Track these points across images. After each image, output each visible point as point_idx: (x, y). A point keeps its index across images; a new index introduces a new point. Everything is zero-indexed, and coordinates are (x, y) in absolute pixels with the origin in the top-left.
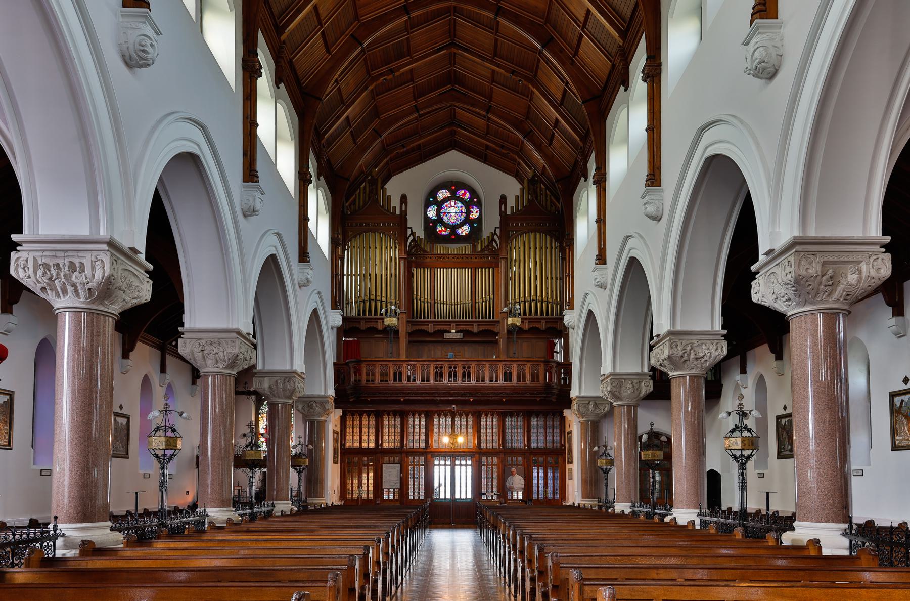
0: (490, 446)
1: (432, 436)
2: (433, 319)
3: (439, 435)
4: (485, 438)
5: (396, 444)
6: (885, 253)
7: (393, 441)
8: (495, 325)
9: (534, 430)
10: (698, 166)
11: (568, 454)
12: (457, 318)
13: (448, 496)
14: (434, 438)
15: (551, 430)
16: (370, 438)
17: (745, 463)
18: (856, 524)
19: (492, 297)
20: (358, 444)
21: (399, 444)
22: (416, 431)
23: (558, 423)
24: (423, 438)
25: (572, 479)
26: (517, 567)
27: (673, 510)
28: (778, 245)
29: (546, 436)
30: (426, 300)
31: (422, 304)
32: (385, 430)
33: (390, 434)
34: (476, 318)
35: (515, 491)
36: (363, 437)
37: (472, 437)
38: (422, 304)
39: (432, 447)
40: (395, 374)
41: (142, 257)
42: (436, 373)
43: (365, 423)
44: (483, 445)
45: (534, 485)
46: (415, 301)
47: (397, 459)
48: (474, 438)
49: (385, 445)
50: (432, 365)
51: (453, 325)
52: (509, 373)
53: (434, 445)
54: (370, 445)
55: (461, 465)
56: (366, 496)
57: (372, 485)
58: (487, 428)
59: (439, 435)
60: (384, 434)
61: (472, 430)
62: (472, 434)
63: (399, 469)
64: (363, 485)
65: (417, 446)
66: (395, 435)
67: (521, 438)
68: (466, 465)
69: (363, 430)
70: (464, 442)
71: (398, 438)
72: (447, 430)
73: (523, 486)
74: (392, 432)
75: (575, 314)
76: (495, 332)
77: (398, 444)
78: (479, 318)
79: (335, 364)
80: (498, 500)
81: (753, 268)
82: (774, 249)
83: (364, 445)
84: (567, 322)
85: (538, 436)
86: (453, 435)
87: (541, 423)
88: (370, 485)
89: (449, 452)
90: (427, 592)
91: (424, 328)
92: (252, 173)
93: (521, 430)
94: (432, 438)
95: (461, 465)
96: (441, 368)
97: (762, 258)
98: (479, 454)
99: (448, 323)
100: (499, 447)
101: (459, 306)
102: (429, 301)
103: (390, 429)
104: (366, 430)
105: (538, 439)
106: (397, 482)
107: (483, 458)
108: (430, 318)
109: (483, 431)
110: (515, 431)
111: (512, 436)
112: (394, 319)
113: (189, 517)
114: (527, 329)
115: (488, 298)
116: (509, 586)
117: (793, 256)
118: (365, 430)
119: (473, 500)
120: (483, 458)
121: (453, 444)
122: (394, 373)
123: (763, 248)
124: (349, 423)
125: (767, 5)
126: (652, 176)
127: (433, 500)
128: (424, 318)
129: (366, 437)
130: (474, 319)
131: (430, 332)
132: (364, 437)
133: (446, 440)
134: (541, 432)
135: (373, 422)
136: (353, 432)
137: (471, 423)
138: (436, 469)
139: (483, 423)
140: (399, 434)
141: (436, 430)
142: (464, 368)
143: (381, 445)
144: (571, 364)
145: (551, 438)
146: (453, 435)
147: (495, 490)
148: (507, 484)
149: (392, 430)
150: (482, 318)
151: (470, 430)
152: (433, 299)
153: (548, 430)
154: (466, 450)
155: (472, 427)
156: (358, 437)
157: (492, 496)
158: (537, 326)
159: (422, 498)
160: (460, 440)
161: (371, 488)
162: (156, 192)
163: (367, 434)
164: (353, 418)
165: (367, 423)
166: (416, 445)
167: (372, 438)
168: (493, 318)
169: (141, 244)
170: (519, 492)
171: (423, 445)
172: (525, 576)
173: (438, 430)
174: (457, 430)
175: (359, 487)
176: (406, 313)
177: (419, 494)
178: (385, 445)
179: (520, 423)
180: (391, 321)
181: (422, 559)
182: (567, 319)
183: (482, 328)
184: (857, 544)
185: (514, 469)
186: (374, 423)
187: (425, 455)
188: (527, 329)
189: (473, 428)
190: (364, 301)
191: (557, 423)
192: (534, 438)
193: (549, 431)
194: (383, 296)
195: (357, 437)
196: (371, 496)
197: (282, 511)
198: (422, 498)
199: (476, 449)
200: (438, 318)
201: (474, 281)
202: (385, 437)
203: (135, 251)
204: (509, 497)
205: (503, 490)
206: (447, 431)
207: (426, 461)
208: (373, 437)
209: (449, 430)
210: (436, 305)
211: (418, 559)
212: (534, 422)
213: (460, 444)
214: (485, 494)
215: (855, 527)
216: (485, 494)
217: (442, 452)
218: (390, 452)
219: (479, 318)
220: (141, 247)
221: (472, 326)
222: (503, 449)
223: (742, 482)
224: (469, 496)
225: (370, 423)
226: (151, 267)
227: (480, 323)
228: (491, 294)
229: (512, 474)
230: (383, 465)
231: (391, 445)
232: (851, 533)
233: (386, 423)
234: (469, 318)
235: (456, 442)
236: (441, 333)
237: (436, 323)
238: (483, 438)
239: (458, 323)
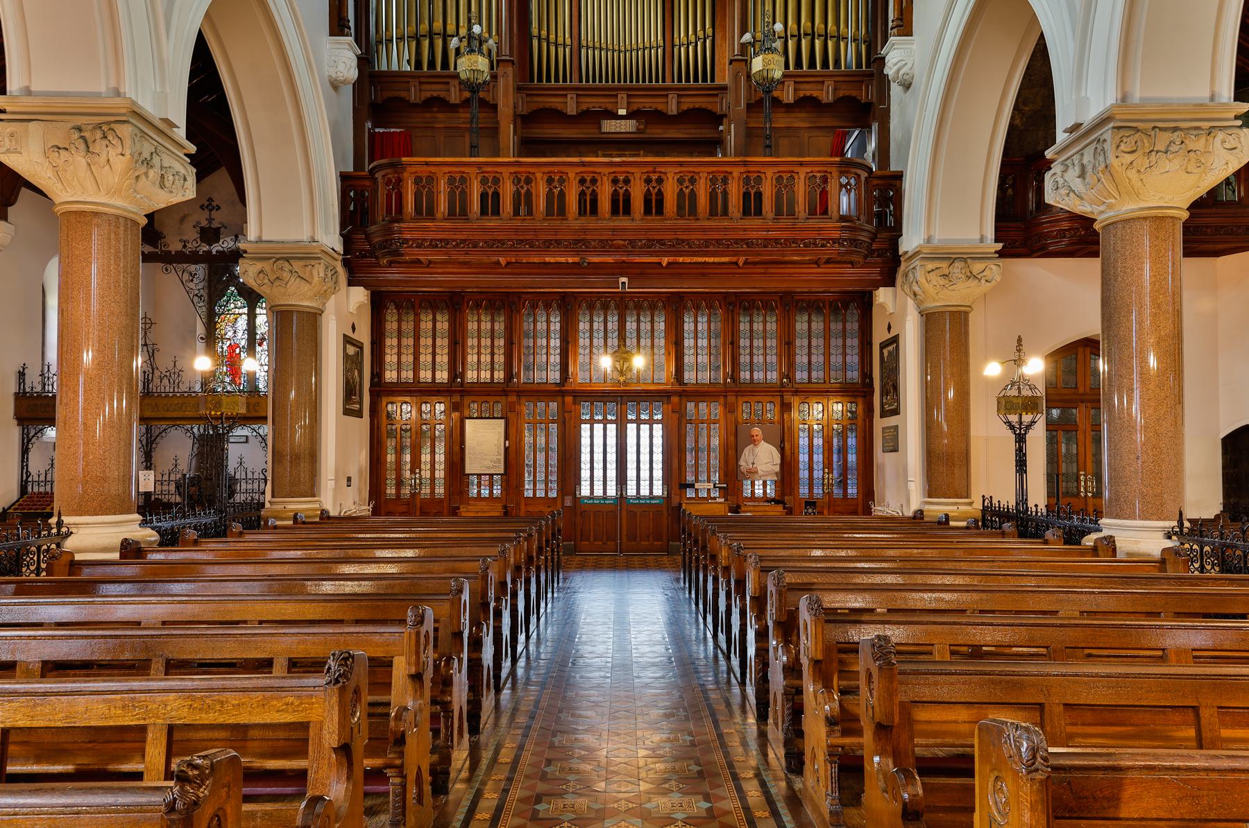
0: (705, 377)
1: (576, 354)
2: (576, 83)
3: (591, 352)
4: (692, 359)
5: (496, 374)
6: (1240, 127)
7: (489, 367)
8: (716, 95)
9: (801, 343)
10: (966, 8)
11: (884, 393)
12: (625, 81)
13: (612, 491)
14: (580, 359)
15: (840, 342)
16: (438, 358)
17: (1025, 434)
18: (1189, 520)
19: (709, 31)
20: (411, 374)
21: (502, 373)
22: (539, 344)
23: (856, 326)
24: (555, 359)
25: (895, 450)
26: (718, 589)
27: (1104, 521)
28: (1091, 114)
29: (827, 354)
30: (560, 40)
31: (553, 49)
32: (472, 342)
33: (483, 350)
34: (673, 82)
35: (747, 479)
36: (422, 358)
37: (663, 359)
38: (553, 49)
39: (575, 380)
40: (484, 196)
41: (181, 133)
42: (518, 193)
43: (426, 325)
44: (689, 376)
45: (801, 466)
46: (535, 42)
47: (498, 407)
48: (668, 360)
49: (471, 376)
50: (572, 175)
51: (622, 97)
52: (755, 193)
53: (580, 376)
54: (438, 375)
55: (639, 422)
56: (428, 491)
57: (442, 466)
58: (696, 338)
59: (591, 352)
60: (469, 350)
61: (663, 342)
62: (663, 351)
63: (502, 430)
64: (423, 466)
65: (541, 379)
66: (492, 354)
67: (772, 359)
68: (651, 422)
69: (422, 342)
70: (647, 368)
71: (500, 359)
72: (610, 341)
73: (777, 469)
74: (486, 346)
75: (914, 47)
76: (714, 114)
77: (499, 375)
78: (680, 80)
79: (344, 178)
80: (722, 500)
81: (1049, 154)
82: (907, 252)
83: (426, 375)
84: (895, 68)
85: (810, 354)
86: (622, 353)
87: (817, 325)
88: (437, 466)
89: (613, 392)
90: (561, 711)
91: (554, 102)
92: (341, 23)
93: (772, 343)
94: (575, 361)
95: (639, 422)
96: (594, 181)
97: (1061, 137)
98: (680, 396)
99: (612, 93)
100: (725, 380)
101: (634, 53)
102: (568, 41)
103: (483, 340)
104: (430, 341)
105: (810, 362)
106: (499, 460)
107: (688, 404)
108: (571, 81)
109: (688, 342)
110: (758, 343)
111: (751, 354)
112: (480, 59)
113: (184, 517)
114: (792, 102)
115: (700, 34)
116: (705, 619)
117: (1110, 131)
118: (426, 341)
119: (668, 498)
120: (688, 404)
121: (621, 373)
122: (482, 195)
123: (1063, 120)
124: (391, 325)
125: (904, 20)
126: (900, 23)
127: (577, 499)
128: (557, 80)
129: (429, 358)
130: (668, 83)
131: (569, 113)
132: (426, 358)
133: (606, 362)
134: (817, 346)
135: (443, 325)
136: (399, 346)
137: (661, 326)
138: (585, 428)
139: (688, 326)
140: (502, 351)
141: (583, 341)
142: (648, 181)
143: (463, 375)
144: (899, 176)
145: (840, 359)
146: (622, 353)
147: (716, 477)
148: (742, 462)
149: (486, 342)
150: (688, 80)
151: (661, 342)
152: (577, 39)
153: (833, 342)
154: (652, 388)
155: (663, 335)
156: (411, 359)
157: (709, 490)
158: (815, 94)
159: (553, 494)
160: (639, 362)
161: (440, 474)
162: (200, 37)
163: (430, 350)
164: (399, 315)
165: (430, 325)
166: (539, 376)
167: (443, 359)
168: (713, 80)
169: (178, 114)
170: (756, 483)
171: (555, 376)
172: (746, 625)
173: (587, 342)
174: (631, 342)
175: (412, 471)
176: (512, 62)
177: (546, 485)
178: (471, 376)
179: (772, 326)
180: (473, 65)
181: (550, 632)
182: (895, 61)
183: (688, 104)
184: (1191, 548)
185: (757, 431)
186: (446, 325)
187: (560, 398)
188: (792, 102)
189: (666, 338)
190: (417, 38)
191: (852, 326)
192: (801, 359)
193: (836, 342)
194: (461, 24)
195: (408, 359)
196: (440, 491)
197: (296, 515)
198: (553, 494)
199: (672, 384)
200: (587, 81)
201: (670, 10)
202: (472, 358)
203: (172, 125)
204: (747, 492)
205: (732, 477)
206: (609, 343)
207: (563, 409)
208: (446, 358)
209: (613, 341)
210: (583, 51)
211: (546, 627)
212: (801, 325)
213: (638, 372)
214: (692, 486)
215: (1187, 524)
216: (692, 486)
217: (597, 392)
218: (485, 391)
219: (680, 80)
220: (180, 118)
221: (665, 100)
222: (733, 385)
223: (1021, 461)
224: (658, 490)
225: (439, 325)
226: (192, 149)
227: (681, 92)
228: (707, 27)
229: (753, 441)
230: (467, 421)
231: (485, 375)
232: (1182, 534)
233: (472, 326)
234: (657, 81)
235: (630, 369)
236: (593, 117)
237: (581, 92)
238: (688, 359)
239: (631, 92)
